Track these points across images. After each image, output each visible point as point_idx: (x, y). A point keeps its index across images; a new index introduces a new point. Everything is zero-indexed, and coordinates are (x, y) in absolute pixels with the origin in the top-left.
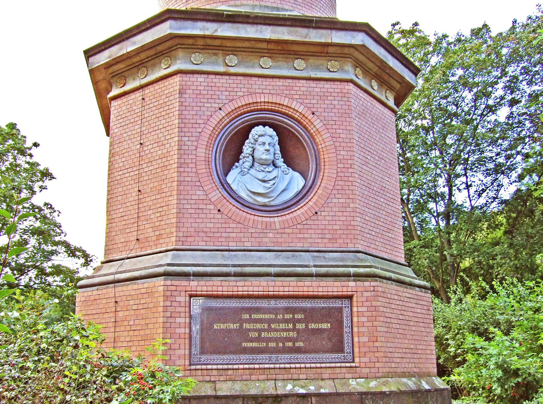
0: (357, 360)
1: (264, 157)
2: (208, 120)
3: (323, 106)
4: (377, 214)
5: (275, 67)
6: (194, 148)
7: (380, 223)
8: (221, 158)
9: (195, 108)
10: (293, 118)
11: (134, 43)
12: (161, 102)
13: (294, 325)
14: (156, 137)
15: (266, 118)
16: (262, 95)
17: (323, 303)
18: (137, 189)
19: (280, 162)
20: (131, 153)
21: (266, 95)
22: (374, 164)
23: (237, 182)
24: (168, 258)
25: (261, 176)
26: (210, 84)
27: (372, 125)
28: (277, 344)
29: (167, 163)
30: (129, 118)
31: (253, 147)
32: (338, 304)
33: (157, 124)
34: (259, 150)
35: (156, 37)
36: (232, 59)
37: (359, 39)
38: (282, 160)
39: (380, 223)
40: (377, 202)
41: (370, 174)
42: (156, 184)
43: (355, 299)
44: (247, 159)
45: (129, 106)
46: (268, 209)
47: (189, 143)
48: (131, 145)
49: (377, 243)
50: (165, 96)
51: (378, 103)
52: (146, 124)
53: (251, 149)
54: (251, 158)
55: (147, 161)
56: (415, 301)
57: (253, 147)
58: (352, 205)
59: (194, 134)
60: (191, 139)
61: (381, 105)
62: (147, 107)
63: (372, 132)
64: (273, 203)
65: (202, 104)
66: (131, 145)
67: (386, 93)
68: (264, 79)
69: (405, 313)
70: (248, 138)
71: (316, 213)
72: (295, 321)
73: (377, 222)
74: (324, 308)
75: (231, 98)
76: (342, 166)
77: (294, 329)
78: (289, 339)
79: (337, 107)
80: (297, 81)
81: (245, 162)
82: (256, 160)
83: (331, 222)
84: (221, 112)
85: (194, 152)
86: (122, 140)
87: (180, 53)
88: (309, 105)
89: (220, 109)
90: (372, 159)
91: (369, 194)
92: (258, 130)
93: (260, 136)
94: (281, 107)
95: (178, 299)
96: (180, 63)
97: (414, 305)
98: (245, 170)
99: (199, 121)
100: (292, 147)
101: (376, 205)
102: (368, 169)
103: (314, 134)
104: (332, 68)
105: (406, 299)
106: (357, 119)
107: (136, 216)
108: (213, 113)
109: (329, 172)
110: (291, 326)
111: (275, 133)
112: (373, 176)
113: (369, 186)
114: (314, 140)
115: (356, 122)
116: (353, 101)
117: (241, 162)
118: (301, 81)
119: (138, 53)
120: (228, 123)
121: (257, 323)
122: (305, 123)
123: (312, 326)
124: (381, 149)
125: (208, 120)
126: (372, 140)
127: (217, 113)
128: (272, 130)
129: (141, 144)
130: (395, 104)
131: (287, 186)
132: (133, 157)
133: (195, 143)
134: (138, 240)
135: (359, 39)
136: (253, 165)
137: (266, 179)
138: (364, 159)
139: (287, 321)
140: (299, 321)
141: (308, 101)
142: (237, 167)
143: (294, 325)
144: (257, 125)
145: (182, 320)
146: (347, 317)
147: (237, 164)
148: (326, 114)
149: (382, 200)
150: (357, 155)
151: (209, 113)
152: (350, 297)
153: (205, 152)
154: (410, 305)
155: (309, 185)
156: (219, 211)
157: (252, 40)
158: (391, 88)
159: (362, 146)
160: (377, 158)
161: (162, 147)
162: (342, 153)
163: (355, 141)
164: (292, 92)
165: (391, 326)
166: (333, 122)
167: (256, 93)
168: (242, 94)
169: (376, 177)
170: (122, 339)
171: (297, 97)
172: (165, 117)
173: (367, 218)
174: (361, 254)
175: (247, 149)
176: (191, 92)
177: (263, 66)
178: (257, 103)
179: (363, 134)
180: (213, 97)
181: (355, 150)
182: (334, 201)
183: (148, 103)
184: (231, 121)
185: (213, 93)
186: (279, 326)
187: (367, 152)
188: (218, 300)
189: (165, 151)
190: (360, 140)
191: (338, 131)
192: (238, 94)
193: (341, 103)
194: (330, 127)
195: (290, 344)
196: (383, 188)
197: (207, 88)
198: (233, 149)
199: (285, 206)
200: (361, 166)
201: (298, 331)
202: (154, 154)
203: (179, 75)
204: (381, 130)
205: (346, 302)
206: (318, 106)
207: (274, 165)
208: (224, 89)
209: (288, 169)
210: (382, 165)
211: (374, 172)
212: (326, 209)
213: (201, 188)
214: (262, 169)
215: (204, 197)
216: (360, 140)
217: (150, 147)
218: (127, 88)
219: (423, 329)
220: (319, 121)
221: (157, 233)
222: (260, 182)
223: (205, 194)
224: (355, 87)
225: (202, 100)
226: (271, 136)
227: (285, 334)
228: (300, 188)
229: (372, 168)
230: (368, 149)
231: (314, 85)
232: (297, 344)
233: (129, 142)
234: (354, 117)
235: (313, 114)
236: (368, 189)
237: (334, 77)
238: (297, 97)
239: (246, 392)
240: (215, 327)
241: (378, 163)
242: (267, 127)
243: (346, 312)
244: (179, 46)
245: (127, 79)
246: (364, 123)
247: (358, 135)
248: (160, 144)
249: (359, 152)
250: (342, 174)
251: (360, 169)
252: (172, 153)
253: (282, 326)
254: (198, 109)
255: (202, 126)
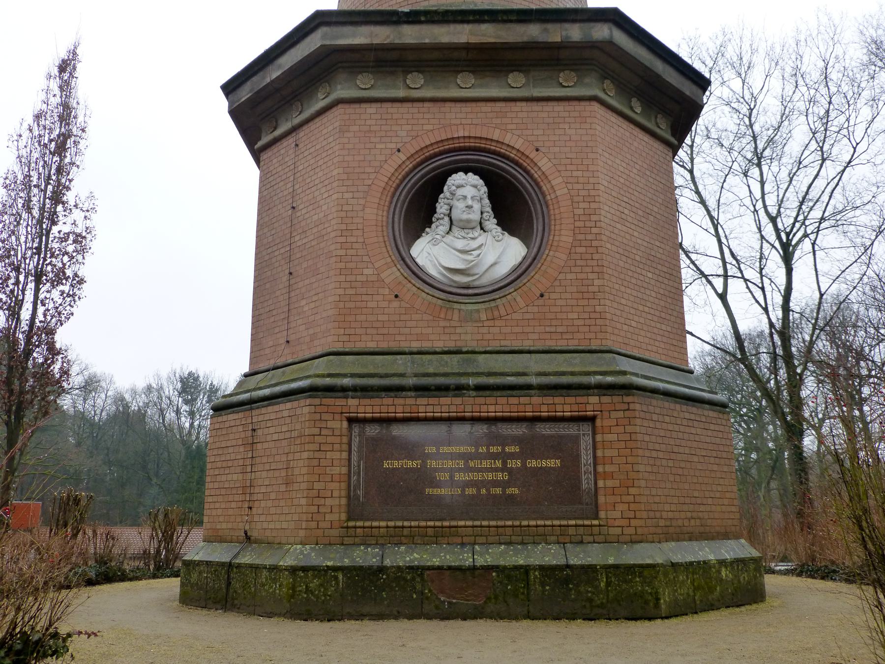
0: (602, 514)
1: (465, 216)
2: (381, 167)
3: (552, 138)
4: (640, 295)
5: (481, 86)
6: (361, 207)
7: (646, 309)
8: (402, 221)
9: (362, 152)
10: (507, 158)
11: (280, 67)
12: (317, 147)
13: (504, 463)
14: (310, 197)
15: (468, 161)
16: (460, 127)
17: (549, 428)
18: (287, 272)
19: (491, 223)
20: (281, 222)
21: (467, 127)
22: (636, 222)
23: (425, 254)
24: (321, 366)
25: (460, 244)
26: (384, 117)
27: (632, 164)
28: (479, 490)
29: (324, 232)
30: (281, 174)
31: (449, 204)
32: (571, 430)
33: (313, 178)
34: (457, 207)
35: (306, 53)
36: (416, 80)
37: (602, 32)
38: (495, 221)
39: (646, 309)
40: (641, 278)
41: (628, 236)
42: (310, 262)
43: (598, 422)
44: (441, 222)
45: (280, 158)
46: (470, 291)
47: (354, 201)
48: (282, 211)
49: (641, 339)
50: (322, 138)
51: (643, 133)
52: (300, 179)
53: (446, 207)
54: (447, 219)
55: (300, 231)
56: (702, 425)
57: (449, 204)
58: (596, 282)
59: (360, 188)
60: (356, 195)
61: (648, 136)
62: (301, 157)
63: (632, 174)
64: (477, 283)
65: (372, 146)
66: (282, 211)
67: (656, 117)
68: (463, 104)
69: (683, 443)
70: (442, 192)
71: (542, 296)
72: (505, 457)
73: (641, 308)
74: (552, 436)
75: (414, 134)
76: (581, 224)
77: (504, 469)
78: (495, 483)
79: (573, 138)
80: (513, 104)
81: (440, 226)
82: (454, 222)
83: (564, 309)
84: (400, 154)
85: (361, 214)
86: (272, 205)
87: (342, 76)
88: (530, 138)
89: (399, 151)
90: (632, 215)
91: (627, 266)
92: (458, 178)
93: (458, 187)
94: (488, 143)
95: (330, 424)
96: (342, 89)
97: (699, 431)
98: (438, 237)
99: (368, 170)
100: (512, 205)
101: (639, 283)
102: (624, 228)
103: (539, 180)
104: (566, 81)
105: (685, 422)
106: (607, 155)
107: (286, 309)
108: (388, 156)
109: (563, 235)
110: (499, 464)
111: (481, 182)
112: (634, 239)
113: (626, 253)
114: (540, 188)
115: (604, 159)
116: (599, 128)
117: (433, 226)
118: (518, 104)
119: (289, 82)
120: (411, 171)
121: (446, 459)
122: (525, 164)
123: (533, 463)
124: (647, 200)
125: (381, 167)
126: (633, 187)
127: (394, 157)
128: (477, 177)
129: (294, 208)
130: (673, 135)
131: (499, 257)
132: (284, 227)
133: (362, 202)
134: (288, 342)
135: (602, 32)
136: (450, 229)
137: (467, 248)
138: (618, 213)
139: (494, 457)
140: (512, 456)
141: (529, 132)
142: (428, 233)
143: (504, 463)
144: (456, 171)
145: (336, 455)
146: (586, 450)
147: (427, 230)
148: (557, 149)
149: (650, 275)
150: (606, 208)
151: (383, 158)
152: (592, 419)
153: (375, 213)
154: (693, 431)
155: (533, 255)
156: (396, 296)
157: (445, 49)
158: (664, 110)
159: (614, 194)
160: (640, 213)
161: (318, 210)
162: (582, 205)
163: (602, 188)
164: (505, 120)
165: (658, 463)
166: (569, 161)
167: (450, 125)
168: (430, 127)
169: (639, 241)
170: (260, 482)
171: (514, 126)
172: (323, 167)
173: (623, 301)
174: (611, 355)
175: (441, 208)
176: (356, 128)
177: (462, 85)
178: (453, 138)
179: (617, 178)
180: (389, 134)
181: (602, 199)
182: (569, 276)
183: (303, 150)
184: (415, 167)
185: (388, 128)
186: (481, 463)
187: (623, 204)
188: (562, 425)
189: (321, 215)
190: (611, 186)
191: (575, 174)
192: (425, 127)
193: (580, 132)
194: (562, 168)
195: (498, 491)
196: (652, 258)
197: (379, 122)
198: (420, 207)
199: (496, 287)
200: (612, 223)
201: (510, 471)
202: (309, 221)
203: (340, 106)
204: (648, 173)
205: (586, 428)
206: (546, 138)
207: (482, 228)
208: (404, 122)
209: (503, 234)
210: (649, 223)
211: (636, 234)
212: (558, 290)
213: (370, 265)
214: (463, 235)
215: (374, 278)
216: (611, 186)
217: (304, 211)
218: (277, 133)
219: (715, 468)
220: (545, 160)
221: (311, 331)
222: (457, 253)
223: (376, 272)
224: (603, 108)
225: (373, 140)
226: (475, 186)
227: (490, 476)
228: (520, 259)
229: (633, 227)
230: (625, 199)
231: (540, 108)
232: (509, 491)
233: (280, 207)
234: (600, 151)
235: (537, 150)
236: (624, 258)
237: (569, 94)
238: (514, 126)
239: (428, 561)
240: (386, 465)
241: (644, 220)
242: (470, 174)
243: (585, 443)
244: (340, 65)
245: (279, 122)
246: (618, 161)
247: (607, 178)
248: (316, 205)
249: (609, 203)
250: (581, 237)
251: (611, 229)
252: (330, 217)
253: (486, 464)
254: (367, 152)
255: (372, 176)
